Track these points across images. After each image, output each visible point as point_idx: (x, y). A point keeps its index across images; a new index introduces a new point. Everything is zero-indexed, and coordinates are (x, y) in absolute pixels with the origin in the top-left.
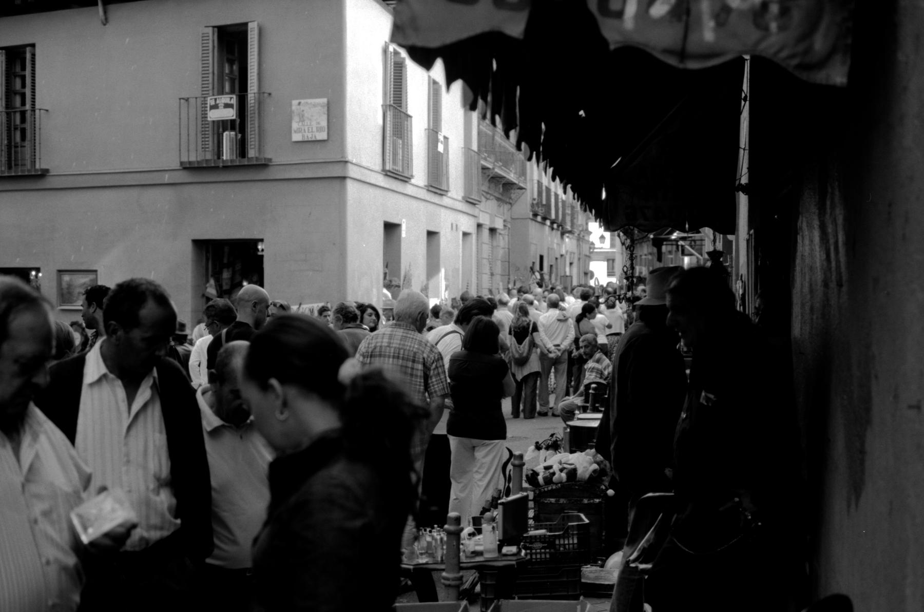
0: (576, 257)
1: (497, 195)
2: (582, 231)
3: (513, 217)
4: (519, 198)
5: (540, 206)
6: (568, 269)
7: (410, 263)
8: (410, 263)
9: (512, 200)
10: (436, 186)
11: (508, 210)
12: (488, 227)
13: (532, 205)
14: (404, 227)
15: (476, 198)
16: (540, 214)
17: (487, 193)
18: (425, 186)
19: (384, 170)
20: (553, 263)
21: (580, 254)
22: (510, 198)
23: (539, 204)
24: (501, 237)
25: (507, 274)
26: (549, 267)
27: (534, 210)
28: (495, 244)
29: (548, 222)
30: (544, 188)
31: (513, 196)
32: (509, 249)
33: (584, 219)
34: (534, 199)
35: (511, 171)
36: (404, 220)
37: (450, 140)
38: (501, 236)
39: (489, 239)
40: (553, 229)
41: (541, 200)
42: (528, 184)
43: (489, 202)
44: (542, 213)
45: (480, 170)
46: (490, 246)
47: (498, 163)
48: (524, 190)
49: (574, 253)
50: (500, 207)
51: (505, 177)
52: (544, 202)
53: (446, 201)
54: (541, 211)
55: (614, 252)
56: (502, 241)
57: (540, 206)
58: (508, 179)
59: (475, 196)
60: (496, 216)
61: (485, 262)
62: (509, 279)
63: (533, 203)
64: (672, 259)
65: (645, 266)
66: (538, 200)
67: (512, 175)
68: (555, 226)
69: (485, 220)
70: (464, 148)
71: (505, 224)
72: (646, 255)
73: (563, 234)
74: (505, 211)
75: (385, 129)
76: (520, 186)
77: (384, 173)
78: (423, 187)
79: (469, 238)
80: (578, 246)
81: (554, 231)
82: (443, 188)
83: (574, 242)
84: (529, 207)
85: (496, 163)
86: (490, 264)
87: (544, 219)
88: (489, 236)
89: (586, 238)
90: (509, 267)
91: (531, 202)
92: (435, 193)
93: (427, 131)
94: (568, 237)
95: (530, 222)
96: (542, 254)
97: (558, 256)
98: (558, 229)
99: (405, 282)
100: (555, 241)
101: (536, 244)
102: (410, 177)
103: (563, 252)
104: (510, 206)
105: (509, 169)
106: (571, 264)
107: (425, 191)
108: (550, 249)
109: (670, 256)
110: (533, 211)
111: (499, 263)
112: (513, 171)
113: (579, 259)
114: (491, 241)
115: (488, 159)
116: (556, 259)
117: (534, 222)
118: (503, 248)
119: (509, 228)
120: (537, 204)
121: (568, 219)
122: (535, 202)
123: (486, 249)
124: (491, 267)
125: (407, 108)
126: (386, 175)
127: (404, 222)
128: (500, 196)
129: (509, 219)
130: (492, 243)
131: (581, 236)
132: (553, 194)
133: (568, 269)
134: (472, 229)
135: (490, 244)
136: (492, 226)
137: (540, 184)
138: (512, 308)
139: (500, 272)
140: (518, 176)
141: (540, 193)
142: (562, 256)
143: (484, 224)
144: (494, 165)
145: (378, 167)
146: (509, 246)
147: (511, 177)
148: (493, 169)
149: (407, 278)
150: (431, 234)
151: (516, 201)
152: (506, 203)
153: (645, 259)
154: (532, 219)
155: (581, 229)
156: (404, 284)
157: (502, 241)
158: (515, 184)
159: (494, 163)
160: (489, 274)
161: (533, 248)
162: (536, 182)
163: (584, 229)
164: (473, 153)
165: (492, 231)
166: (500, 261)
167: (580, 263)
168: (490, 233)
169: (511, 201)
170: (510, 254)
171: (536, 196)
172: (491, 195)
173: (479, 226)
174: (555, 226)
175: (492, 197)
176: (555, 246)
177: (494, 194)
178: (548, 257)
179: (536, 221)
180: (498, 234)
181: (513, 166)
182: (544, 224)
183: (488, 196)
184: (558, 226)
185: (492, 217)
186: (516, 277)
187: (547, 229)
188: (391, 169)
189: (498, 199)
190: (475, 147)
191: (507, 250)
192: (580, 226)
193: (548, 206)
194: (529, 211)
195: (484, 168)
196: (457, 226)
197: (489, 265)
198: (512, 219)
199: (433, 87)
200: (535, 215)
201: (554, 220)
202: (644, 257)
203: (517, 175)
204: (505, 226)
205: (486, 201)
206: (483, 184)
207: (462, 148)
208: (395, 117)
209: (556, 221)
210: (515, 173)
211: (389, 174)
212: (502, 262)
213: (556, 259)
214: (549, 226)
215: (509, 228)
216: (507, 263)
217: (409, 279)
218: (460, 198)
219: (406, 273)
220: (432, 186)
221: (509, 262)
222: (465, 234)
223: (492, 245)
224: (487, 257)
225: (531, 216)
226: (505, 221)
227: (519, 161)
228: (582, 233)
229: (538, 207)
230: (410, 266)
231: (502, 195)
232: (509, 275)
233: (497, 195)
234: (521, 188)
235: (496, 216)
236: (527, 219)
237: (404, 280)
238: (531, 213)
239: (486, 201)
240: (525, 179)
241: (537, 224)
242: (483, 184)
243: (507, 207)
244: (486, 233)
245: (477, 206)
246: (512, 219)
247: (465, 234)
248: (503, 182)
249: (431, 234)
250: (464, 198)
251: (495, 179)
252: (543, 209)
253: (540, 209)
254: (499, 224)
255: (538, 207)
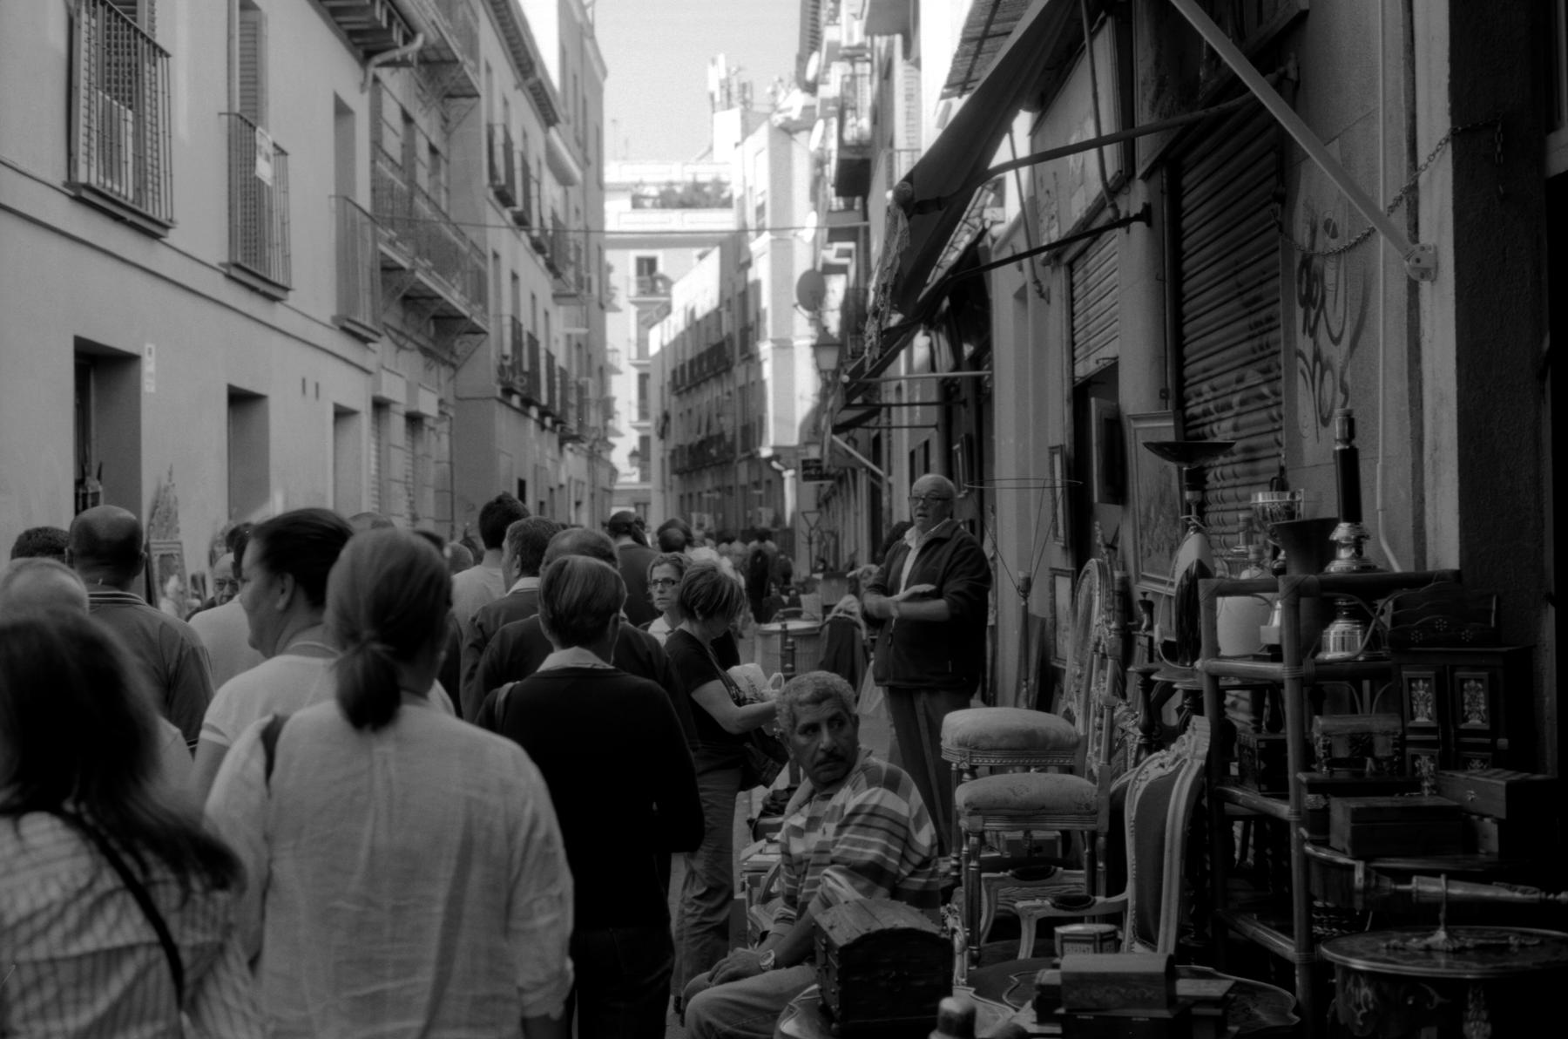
0: (587, 490)
1: (423, 341)
2: (596, 440)
3: (460, 396)
4: (473, 352)
5: (517, 372)
6: (572, 513)
7: (171, 467)
8: (171, 467)
9: (457, 357)
10: (253, 269)
11: (449, 380)
12: (402, 410)
13: (501, 370)
14: (149, 367)
15: (368, 323)
16: (519, 390)
17: (400, 333)
18: (222, 265)
19: (70, 183)
20: (545, 498)
21: (593, 486)
22: (453, 353)
23: (516, 366)
24: (434, 439)
25: (449, 518)
26: (538, 505)
27: (504, 379)
28: (420, 450)
29: (534, 412)
30: (525, 338)
31: (459, 349)
32: (451, 463)
33: (601, 417)
34: (505, 358)
35: (454, 286)
36: (148, 346)
37: (293, 161)
38: (432, 433)
39: (407, 439)
40: (543, 427)
41: (520, 363)
42: (492, 325)
43: (403, 353)
44: (523, 388)
45: (378, 275)
46: (410, 455)
47: (423, 260)
48: (482, 336)
49: (583, 484)
50: (431, 369)
51: (440, 297)
52: (526, 367)
53: (278, 315)
54: (519, 383)
55: (648, 491)
56: (438, 444)
57: (517, 372)
58: (448, 304)
59: (364, 317)
60: (420, 385)
61: (398, 489)
62: (453, 528)
63: (502, 367)
64: (760, 496)
65: (709, 512)
66: (513, 358)
67: (456, 295)
68: (548, 421)
69: (393, 389)
70: (337, 196)
71: (443, 408)
72: (709, 492)
73: (561, 444)
74: (442, 381)
75: (75, 61)
76: (474, 324)
77: (72, 193)
78: (215, 264)
79: (351, 425)
80: (591, 470)
81: (546, 432)
82: (273, 278)
83: (582, 462)
84: (494, 373)
85: (417, 259)
86: (410, 495)
87: (527, 402)
88: (407, 433)
89: (604, 455)
90: (452, 503)
91: (498, 363)
92: (253, 289)
93: (225, 118)
94: (571, 450)
95: (496, 403)
96: (523, 477)
97: (555, 486)
98: (553, 430)
99: (155, 521)
100: (549, 453)
101: (510, 456)
102: (168, 223)
103: (563, 480)
104: (452, 371)
105: (449, 281)
106: (578, 504)
107: (220, 278)
108: (537, 469)
109: (757, 492)
110: (502, 383)
111: (430, 494)
112: (459, 287)
113: (592, 496)
114: (410, 443)
115: (398, 244)
116: (551, 490)
117: (504, 407)
118: (438, 462)
119: (451, 419)
120: (512, 368)
121: (572, 413)
122: (508, 363)
123: (399, 463)
124: (412, 503)
125: (152, 20)
126: (78, 199)
127: (150, 353)
128: (430, 346)
129: (451, 400)
130: (413, 447)
131: (595, 450)
132: (542, 354)
133: (572, 513)
134: (363, 406)
135: (409, 449)
136: (414, 408)
137: (517, 326)
138: (404, 695)
139: (432, 514)
140: (468, 301)
141: (517, 345)
142: (561, 486)
143: (394, 402)
144: (414, 263)
145: (59, 178)
146: (451, 456)
147: (452, 298)
148: (412, 271)
149: (162, 508)
150: (241, 401)
151: (466, 360)
152: (444, 363)
153: (709, 499)
154: (500, 401)
155: (594, 436)
156: (150, 524)
157: (438, 444)
158: (464, 317)
159: (413, 258)
160: (407, 516)
161: (503, 461)
162: (507, 321)
163: (601, 437)
164: (358, 214)
165: (414, 420)
166: (432, 490)
167: (593, 503)
168: (407, 426)
169: (454, 360)
170: (456, 477)
171: (508, 350)
172: (409, 338)
173: (380, 406)
174: (548, 421)
175: (409, 345)
176: (549, 464)
177: (415, 338)
178: (536, 486)
179: (510, 406)
180: (426, 429)
181: (458, 275)
182: (527, 415)
183: (402, 341)
184: (555, 423)
185: (412, 389)
186: (468, 524)
187: (532, 425)
188: (93, 182)
189: (425, 351)
190: (364, 199)
191: (446, 466)
192: (594, 429)
193: (534, 375)
194: (493, 384)
195: (389, 269)
196: (317, 386)
197: (406, 497)
198: (458, 399)
199: (241, 15)
200: (508, 391)
201: (546, 407)
202: (705, 495)
203: (466, 296)
204: (441, 413)
205: (397, 352)
206: (385, 310)
207: (330, 197)
208: (110, 46)
209: (552, 411)
210: (463, 293)
211: (85, 194)
212: (437, 491)
213: (551, 490)
214: (537, 421)
215: (451, 419)
216: (448, 495)
217: (169, 511)
218: (327, 320)
219: (158, 492)
220: (238, 266)
221: (452, 493)
222: (342, 414)
223: (413, 453)
224: (403, 479)
225: (499, 394)
226: (441, 402)
227: (472, 272)
228: (597, 444)
229: (514, 375)
230: (170, 473)
231: (434, 342)
232: (453, 520)
233: (423, 341)
234: (477, 331)
235: (420, 385)
236: (488, 398)
237: (152, 515)
238: (499, 388)
239: (397, 352)
240: (486, 310)
241: (512, 413)
242: (385, 310)
243: (445, 372)
244: (397, 424)
245: (371, 345)
246: (458, 399)
247: (342, 414)
248: (434, 310)
249: (241, 401)
250: (335, 319)
251: (415, 301)
252: (525, 380)
253: (518, 377)
254: (428, 405)
255: (514, 375)
